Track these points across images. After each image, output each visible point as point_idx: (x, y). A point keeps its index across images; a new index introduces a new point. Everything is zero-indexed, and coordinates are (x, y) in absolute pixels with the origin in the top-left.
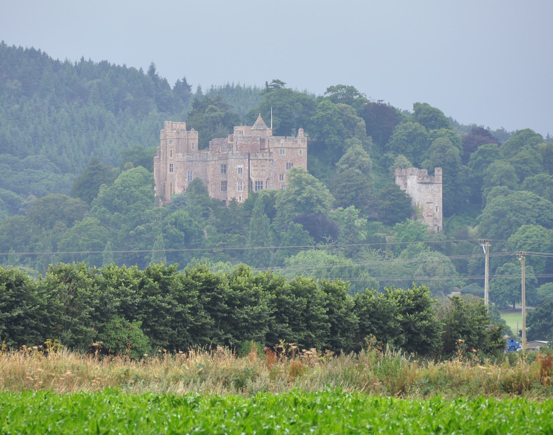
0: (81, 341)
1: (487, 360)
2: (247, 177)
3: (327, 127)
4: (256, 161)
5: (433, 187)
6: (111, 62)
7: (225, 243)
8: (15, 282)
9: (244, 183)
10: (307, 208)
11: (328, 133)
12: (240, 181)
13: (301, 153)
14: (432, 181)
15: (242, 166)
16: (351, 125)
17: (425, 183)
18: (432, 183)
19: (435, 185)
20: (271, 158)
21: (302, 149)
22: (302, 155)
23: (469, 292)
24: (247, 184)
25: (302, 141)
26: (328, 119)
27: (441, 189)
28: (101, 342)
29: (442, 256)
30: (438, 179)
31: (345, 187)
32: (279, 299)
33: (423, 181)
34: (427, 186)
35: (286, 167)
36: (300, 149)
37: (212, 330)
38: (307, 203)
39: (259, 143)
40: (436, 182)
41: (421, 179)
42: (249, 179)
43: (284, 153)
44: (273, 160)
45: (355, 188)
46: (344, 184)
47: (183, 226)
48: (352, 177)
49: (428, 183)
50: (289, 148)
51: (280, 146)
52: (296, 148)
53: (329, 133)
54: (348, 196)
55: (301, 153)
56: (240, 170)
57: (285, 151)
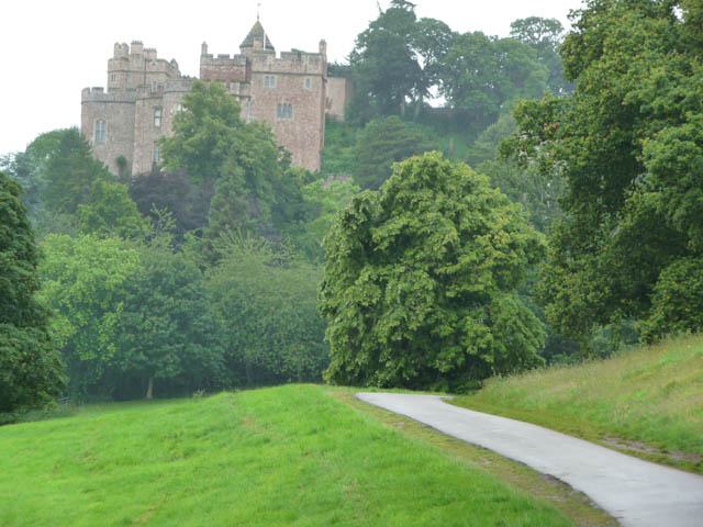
0: (210, 296)
4: (308, 72)
6: (487, 33)
13: (308, 84)
20: (245, 93)
21: (311, 78)
22: (310, 89)
23: (212, 430)
25: (311, 60)
28: (361, 335)
32: (479, 359)
35: (275, 112)
36: (306, 78)
43: (272, 83)
44: (250, 97)
50: (284, 74)
51: (266, 70)
52: (300, 75)
55: (308, 84)
57: (276, 81)
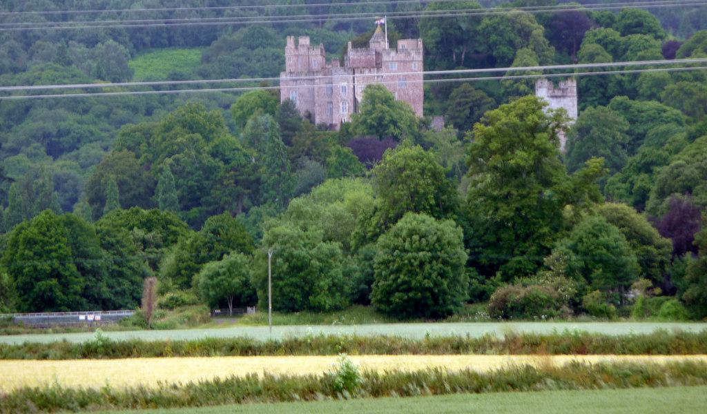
1: (393, 373)
2: (351, 96)
3: (494, 37)
5: (565, 100)
7: (238, 173)
8: (191, 256)
9: (348, 103)
10: (381, 131)
11: (495, 44)
12: (344, 101)
14: (565, 94)
15: (345, 84)
16: (525, 34)
17: (557, 97)
18: (564, 97)
19: (569, 99)
24: (351, 105)
26: (495, 29)
27: (576, 103)
29: (68, 155)
30: (572, 92)
31: (459, 104)
33: (553, 94)
34: (559, 99)
37: (127, 303)
38: (380, 124)
39: (374, 57)
40: (570, 95)
41: (550, 92)
42: (355, 99)
45: (470, 105)
46: (458, 100)
47: (225, 156)
48: (470, 92)
49: (560, 97)
50: (401, 61)
51: (391, 59)
53: (496, 45)
54: (462, 115)
55: (415, 67)
56: (344, 89)
